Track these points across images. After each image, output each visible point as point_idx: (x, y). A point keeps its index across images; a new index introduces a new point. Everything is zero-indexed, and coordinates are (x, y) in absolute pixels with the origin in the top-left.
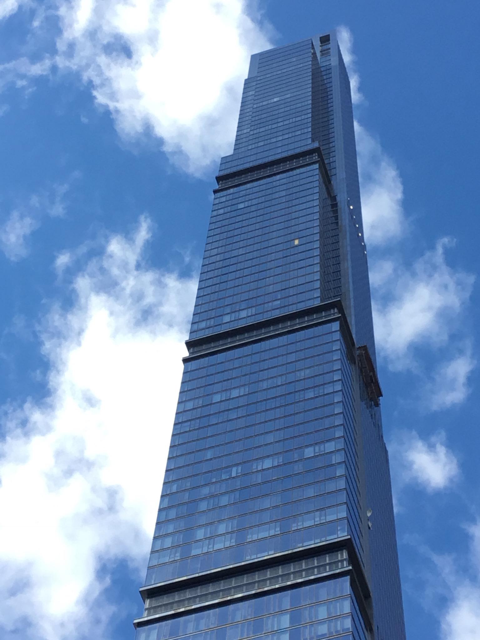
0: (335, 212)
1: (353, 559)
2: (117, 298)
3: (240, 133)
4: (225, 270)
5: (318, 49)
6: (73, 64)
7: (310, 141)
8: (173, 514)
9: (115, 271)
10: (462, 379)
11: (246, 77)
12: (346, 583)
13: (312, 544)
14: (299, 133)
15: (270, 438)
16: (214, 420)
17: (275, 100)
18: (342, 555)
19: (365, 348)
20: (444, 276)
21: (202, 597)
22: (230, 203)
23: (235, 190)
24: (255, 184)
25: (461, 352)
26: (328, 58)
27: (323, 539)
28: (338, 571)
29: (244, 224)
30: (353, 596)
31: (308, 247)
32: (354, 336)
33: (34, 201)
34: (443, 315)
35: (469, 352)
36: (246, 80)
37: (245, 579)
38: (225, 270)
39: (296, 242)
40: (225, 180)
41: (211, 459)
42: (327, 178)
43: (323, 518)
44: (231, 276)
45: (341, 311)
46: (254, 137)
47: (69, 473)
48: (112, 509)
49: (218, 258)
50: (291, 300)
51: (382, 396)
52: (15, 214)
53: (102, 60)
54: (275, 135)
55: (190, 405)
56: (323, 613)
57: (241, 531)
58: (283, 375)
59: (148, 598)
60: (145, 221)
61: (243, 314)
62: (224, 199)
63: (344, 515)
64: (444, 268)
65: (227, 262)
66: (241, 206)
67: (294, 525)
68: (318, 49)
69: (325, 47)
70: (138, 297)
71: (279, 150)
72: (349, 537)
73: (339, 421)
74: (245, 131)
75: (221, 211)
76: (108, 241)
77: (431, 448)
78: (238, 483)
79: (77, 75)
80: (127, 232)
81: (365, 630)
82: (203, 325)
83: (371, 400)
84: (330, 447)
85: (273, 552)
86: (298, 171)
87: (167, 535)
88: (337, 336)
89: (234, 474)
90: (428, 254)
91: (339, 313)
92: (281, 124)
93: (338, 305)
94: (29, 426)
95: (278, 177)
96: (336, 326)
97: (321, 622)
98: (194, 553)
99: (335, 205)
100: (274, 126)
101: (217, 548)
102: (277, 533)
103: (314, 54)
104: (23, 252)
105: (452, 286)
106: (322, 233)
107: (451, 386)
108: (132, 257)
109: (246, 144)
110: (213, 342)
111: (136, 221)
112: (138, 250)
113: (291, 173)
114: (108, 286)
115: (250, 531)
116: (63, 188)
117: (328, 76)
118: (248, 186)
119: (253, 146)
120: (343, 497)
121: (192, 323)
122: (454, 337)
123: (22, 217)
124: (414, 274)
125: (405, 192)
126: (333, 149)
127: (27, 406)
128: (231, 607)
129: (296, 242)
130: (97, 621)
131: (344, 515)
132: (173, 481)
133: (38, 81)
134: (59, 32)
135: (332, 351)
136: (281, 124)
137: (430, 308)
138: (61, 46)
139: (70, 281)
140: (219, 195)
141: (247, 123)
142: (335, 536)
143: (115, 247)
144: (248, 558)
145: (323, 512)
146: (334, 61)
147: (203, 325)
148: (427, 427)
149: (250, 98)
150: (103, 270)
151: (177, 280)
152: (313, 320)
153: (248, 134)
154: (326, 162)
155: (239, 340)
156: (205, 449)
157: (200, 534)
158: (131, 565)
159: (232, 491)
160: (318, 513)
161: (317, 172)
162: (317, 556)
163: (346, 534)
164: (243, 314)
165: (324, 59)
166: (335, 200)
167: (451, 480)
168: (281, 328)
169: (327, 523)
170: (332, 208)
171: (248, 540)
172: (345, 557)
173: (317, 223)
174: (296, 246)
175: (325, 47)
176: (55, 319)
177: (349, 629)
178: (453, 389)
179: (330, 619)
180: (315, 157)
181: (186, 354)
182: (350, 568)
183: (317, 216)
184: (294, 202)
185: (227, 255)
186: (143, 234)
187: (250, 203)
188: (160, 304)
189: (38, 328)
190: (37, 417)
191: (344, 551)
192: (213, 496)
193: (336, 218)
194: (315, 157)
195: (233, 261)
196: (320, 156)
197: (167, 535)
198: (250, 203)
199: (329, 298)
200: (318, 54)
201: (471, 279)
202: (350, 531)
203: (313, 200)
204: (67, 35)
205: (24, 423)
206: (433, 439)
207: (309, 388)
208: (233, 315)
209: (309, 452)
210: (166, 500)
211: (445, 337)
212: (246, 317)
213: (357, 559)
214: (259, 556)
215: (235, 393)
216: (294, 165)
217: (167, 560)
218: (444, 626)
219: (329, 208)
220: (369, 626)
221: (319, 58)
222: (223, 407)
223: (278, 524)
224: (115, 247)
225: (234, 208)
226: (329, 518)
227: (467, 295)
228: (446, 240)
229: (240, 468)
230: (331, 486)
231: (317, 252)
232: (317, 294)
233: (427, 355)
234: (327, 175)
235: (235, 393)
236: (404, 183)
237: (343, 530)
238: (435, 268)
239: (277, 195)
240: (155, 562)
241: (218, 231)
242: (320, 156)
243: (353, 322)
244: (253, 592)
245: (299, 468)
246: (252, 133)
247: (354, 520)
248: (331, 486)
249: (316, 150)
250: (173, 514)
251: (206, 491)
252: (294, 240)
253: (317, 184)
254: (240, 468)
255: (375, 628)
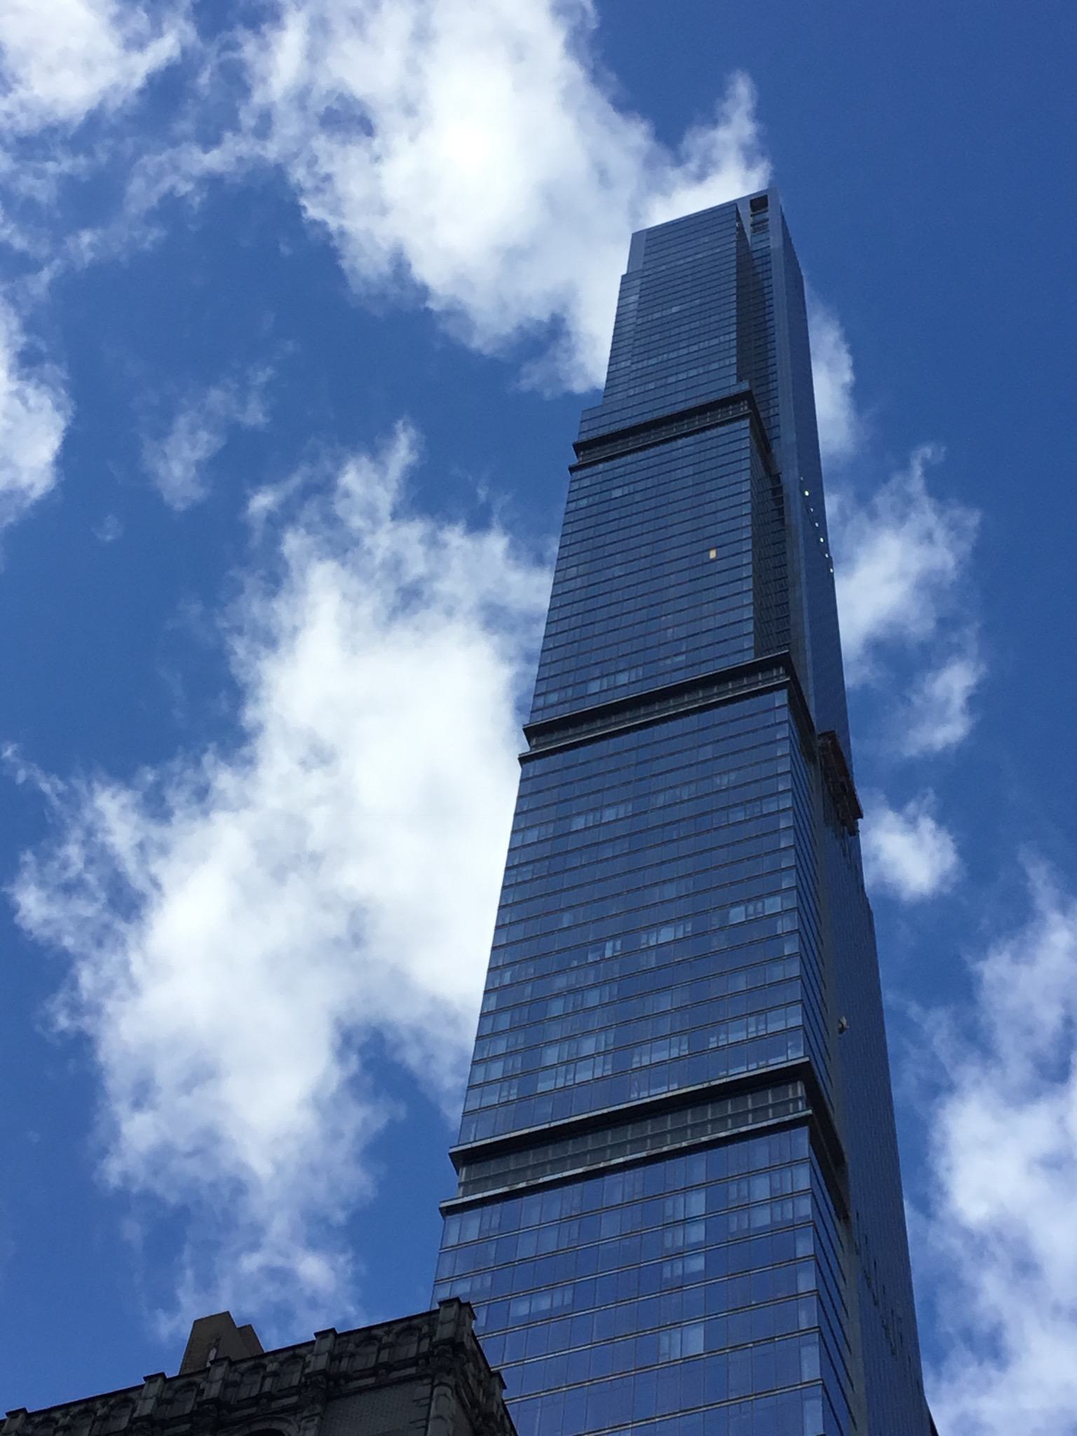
0: (780, 501)
1: (815, 1097)
2: (357, 570)
3: (614, 368)
4: (591, 604)
5: (747, 221)
6: (272, 151)
7: (734, 380)
8: (504, 1021)
9: (357, 522)
10: (958, 700)
11: (625, 272)
12: (802, 1138)
13: (741, 1072)
14: (715, 366)
15: (670, 891)
16: (575, 861)
17: (674, 310)
18: (795, 1092)
19: (831, 735)
20: (926, 516)
21: (559, 1164)
22: (598, 488)
23: (607, 465)
24: (641, 455)
25: (957, 651)
26: (764, 237)
27: (761, 1063)
28: (787, 1118)
29: (624, 523)
30: (813, 1156)
31: (734, 561)
32: (813, 715)
33: (216, 396)
34: (928, 586)
35: (973, 648)
36: (623, 277)
37: (630, 1132)
38: (591, 604)
39: (713, 554)
40: (589, 448)
41: (569, 928)
42: (763, 442)
43: (762, 1027)
44: (603, 614)
45: (790, 671)
46: (639, 373)
47: (279, 873)
48: (357, 939)
49: (579, 582)
50: (703, 655)
51: (861, 817)
52: (182, 422)
53: (321, 143)
54: (675, 370)
55: (532, 836)
56: (761, 1188)
57: (622, 1049)
58: (690, 782)
59: (464, 1165)
60: (405, 430)
61: (623, 678)
62: (586, 482)
63: (796, 1021)
64: (926, 503)
65: (593, 591)
66: (617, 493)
67: (712, 1040)
68: (747, 221)
69: (758, 218)
70: (395, 565)
71: (681, 397)
72: (807, 1059)
73: (788, 861)
74: (623, 364)
75: (584, 503)
76: (339, 465)
77: (912, 823)
78: (616, 968)
79: (279, 171)
80: (371, 442)
81: (835, 1218)
82: (553, 698)
83: (843, 823)
84: (774, 905)
85: (676, 1086)
86: (714, 432)
87: (496, 1058)
88: (784, 715)
89: (608, 954)
90: (896, 479)
91: (787, 674)
92: (685, 351)
93: (785, 662)
94: (213, 796)
95: (680, 442)
96: (781, 698)
97: (760, 1204)
98: (542, 1087)
99: (777, 490)
100: (672, 355)
101: (580, 1073)
102: (683, 1053)
103: (741, 229)
104: (198, 493)
105: (940, 534)
106: (755, 538)
107: (940, 713)
108: (385, 497)
109: (626, 386)
110: (572, 726)
111: (390, 433)
112: (395, 486)
113: (702, 436)
114: (342, 546)
115: (637, 1050)
116: (262, 376)
117: (765, 267)
118: (629, 458)
119: (637, 390)
120: (796, 992)
121: (536, 696)
122: (946, 623)
123: (192, 431)
124: (873, 515)
125: (856, 368)
126: (774, 393)
127: (208, 759)
128: (608, 1179)
129: (713, 554)
130: (335, 1136)
131: (796, 1021)
132: (506, 966)
133: (212, 181)
134: (246, 91)
135: (775, 742)
136: (685, 351)
137: (903, 575)
138: (247, 120)
139: (274, 541)
140: (578, 474)
141: (625, 350)
142: (783, 1059)
143: (354, 478)
144: (635, 1096)
145: (762, 1018)
146: (774, 242)
147: (553, 698)
148: (903, 789)
149: (632, 307)
150: (332, 521)
151: (462, 537)
152: (741, 688)
153: (627, 371)
154: (762, 415)
155: (616, 724)
156: (562, 910)
157: (551, 1056)
158: (389, 1036)
159: (604, 983)
160: (752, 1020)
161: (747, 433)
162: (751, 1093)
163: (802, 1054)
164: (623, 678)
165: (756, 239)
166: (779, 480)
167: (944, 879)
168: (688, 702)
169: (770, 1034)
170: (774, 494)
171: (634, 1066)
172: (800, 1094)
173: (747, 521)
174: (713, 561)
175: (758, 218)
176: (255, 607)
177: (807, 1216)
178: (943, 720)
179: (777, 1199)
180: (744, 408)
181: (524, 747)
182: (810, 1112)
183: (747, 509)
184: (708, 486)
185: (595, 578)
186: (402, 451)
187: (631, 488)
188: (433, 577)
189: (222, 624)
190: (225, 780)
191: (799, 1083)
192: (573, 991)
193: (781, 511)
194: (744, 408)
195: (606, 587)
196: (752, 405)
197: (496, 1058)
198: (631, 488)
199: (768, 650)
200: (748, 230)
201: (973, 519)
202: (809, 1050)
203: (741, 486)
204: (258, 98)
205: (202, 794)
206: (911, 807)
207: (736, 805)
208: (605, 680)
209: (737, 915)
210: (493, 998)
211: (930, 625)
212: (626, 683)
213: (819, 1091)
214: (653, 1092)
215: (609, 815)
216: (708, 421)
217: (494, 1100)
218: (936, 1137)
219: (769, 495)
220: (842, 1212)
221: (749, 236)
222: (590, 837)
223: (685, 1038)
224: (354, 478)
225: (605, 496)
226: (772, 1028)
227: (966, 547)
228: (927, 451)
229: (618, 943)
230: (777, 973)
231: (748, 571)
232: (748, 643)
233: (902, 658)
234: (764, 438)
235: (609, 815)
236: (852, 351)
237: (796, 1047)
238: (908, 501)
239: (679, 474)
240: (474, 1105)
241: (579, 536)
242: (752, 405)
243: (811, 692)
244: (644, 1154)
245: (718, 943)
246: (634, 367)
247: (812, 1031)
248: (777, 973)
249: (746, 396)
250: (504, 1021)
251: (561, 983)
252: (709, 550)
253: (747, 454)
254: (618, 943)
255: (852, 1215)
